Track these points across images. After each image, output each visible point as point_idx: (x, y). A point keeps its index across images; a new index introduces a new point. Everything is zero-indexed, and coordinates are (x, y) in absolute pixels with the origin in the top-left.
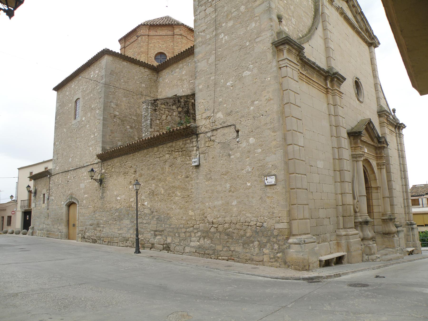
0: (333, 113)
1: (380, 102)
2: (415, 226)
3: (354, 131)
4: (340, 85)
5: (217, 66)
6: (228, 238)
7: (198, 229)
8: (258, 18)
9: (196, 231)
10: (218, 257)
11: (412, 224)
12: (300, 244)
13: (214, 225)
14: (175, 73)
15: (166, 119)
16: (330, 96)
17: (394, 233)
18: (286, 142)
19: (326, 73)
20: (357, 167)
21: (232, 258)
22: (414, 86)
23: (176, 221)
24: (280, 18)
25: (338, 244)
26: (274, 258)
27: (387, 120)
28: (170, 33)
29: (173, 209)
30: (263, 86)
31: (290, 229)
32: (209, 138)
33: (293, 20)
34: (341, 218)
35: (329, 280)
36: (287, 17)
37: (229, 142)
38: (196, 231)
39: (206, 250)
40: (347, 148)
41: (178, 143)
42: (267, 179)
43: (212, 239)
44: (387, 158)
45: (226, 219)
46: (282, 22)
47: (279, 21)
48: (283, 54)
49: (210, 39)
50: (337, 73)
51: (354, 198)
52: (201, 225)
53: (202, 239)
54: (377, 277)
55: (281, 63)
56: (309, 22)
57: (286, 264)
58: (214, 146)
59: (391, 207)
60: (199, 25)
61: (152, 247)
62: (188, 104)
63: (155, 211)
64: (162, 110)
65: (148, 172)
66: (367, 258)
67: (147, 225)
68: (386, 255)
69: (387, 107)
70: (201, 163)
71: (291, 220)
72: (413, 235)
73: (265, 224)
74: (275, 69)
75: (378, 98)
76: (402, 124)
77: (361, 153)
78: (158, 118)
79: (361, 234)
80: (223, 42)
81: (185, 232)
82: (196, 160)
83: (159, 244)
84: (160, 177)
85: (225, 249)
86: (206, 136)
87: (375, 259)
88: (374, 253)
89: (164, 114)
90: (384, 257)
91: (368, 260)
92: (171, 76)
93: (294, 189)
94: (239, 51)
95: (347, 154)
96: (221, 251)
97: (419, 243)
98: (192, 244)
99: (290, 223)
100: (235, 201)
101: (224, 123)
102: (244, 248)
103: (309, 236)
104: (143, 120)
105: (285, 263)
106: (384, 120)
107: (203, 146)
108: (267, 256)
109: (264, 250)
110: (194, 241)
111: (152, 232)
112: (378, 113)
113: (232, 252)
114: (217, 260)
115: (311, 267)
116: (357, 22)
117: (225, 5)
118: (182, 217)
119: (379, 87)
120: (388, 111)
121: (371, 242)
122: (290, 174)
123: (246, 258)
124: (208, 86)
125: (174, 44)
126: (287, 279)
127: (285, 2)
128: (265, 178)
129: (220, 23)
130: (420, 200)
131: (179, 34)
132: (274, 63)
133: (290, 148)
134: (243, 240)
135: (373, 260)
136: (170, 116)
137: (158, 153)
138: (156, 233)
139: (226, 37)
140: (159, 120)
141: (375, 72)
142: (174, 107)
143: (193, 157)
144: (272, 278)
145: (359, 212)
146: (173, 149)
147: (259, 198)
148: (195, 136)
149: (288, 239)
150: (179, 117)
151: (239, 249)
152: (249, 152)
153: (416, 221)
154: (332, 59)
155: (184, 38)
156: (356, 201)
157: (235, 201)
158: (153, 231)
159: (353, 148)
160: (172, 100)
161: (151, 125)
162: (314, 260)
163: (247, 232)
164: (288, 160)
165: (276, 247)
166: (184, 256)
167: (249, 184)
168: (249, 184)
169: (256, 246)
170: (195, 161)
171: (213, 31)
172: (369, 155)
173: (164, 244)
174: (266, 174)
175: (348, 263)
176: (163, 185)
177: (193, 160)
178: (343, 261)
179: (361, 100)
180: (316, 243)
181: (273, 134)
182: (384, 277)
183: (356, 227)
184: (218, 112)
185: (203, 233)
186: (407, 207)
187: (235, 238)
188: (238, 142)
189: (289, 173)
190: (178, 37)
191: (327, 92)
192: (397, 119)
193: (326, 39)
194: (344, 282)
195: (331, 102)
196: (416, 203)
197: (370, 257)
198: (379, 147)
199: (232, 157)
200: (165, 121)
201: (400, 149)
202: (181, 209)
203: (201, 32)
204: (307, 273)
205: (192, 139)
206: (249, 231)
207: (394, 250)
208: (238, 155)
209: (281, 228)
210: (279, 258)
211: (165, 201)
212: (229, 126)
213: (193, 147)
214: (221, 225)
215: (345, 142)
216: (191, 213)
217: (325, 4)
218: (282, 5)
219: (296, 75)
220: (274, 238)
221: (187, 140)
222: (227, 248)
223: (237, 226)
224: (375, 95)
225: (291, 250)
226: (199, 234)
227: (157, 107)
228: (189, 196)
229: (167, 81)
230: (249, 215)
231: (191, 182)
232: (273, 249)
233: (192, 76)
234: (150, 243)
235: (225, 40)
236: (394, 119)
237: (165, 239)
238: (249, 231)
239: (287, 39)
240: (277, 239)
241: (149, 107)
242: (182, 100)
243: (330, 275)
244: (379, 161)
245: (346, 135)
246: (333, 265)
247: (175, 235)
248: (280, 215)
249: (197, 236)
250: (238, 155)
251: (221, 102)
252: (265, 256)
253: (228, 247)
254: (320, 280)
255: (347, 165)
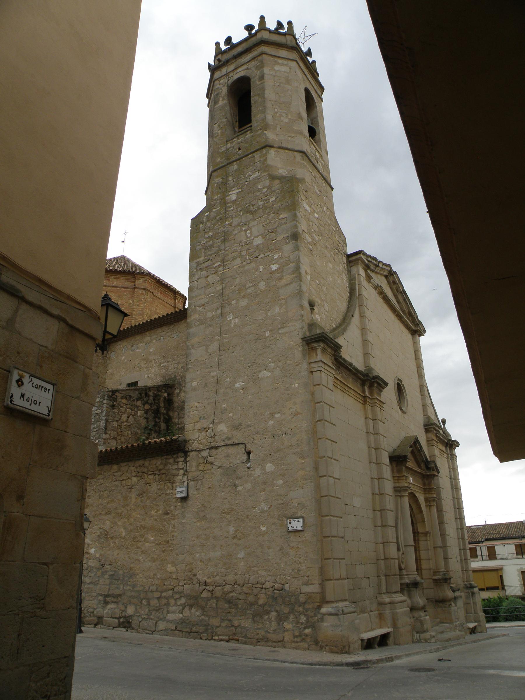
0: (372, 430)
1: (427, 411)
2: (476, 590)
3: (397, 454)
4: (381, 391)
5: (221, 357)
6: (230, 607)
7: (181, 593)
8: (283, 302)
9: (177, 596)
10: (212, 636)
11: (472, 587)
12: (337, 615)
13: (207, 588)
14: (138, 348)
15: (127, 421)
16: (369, 407)
17: (450, 600)
18: (318, 473)
19: (364, 376)
20: (401, 504)
21: (236, 637)
22: (495, 454)
23: (145, 580)
24: (312, 305)
25: (381, 616)
26: (300, 636)
27: (437, 436)
28: (130, 284)
29: (139, 560)
30: (288, 395)
31: (323, 593)
32: (204, 458)
33: (326, 306)
34: (383, 578)
35: (380, 665)
36: (319, 301)
37: (236, 468)
38: (177, 596)
39: (194, 625)
40: (389, 478)
41: (154, 461)
42: (290, 523)
43: (203, 608)
44: (438, 491)
45: (227, 578)
46: (314, 309)
47: (311, 309)
48: (317, 355)
49: (212, 318)
50: (377, 377)
51: (399, 549)
52: (187, 586)
53: (187, 608)
54: (440, 660)
55: (313, 365)
56: (343, 306)
57: (318, 644)
58: (212, 471)
59: (445, 562)
60: (196, 296)
61: (99, 621)
62: (159, 400)
63: (107, 563)
64: (122, 407)
65: (100, 501)
66: (418, 638)
67: (91, 586)
68: (442, 632)
69: (436, 418)
70: (190, 494)
71: (324, 579)
72: (475, 603)
73: (287, 587)
74: (306, 373)
75: (424, 406)
76: (455, 441)
77: (406, 485)
78: (116, 419)
79: (409, 601)
80: (232, 326)
81: (158, 598)
82: (183, 489)
83: (112, 617)
84: (119, 511)
85: (224, 624)
86: (200, 456)
87: (429, 639)
88: (427, 629)
89: (124, 413)
90: (440, 636)
91: (419, 641)
92: (131, 353)
93: (329, 537)
94: (254, 342)
95: (388, 487)
96: (217, 627)
97: (482, 615)
98: (170, 616)
99: (322, 585)
100: (243, 553)
101: (229, 439)
102: (254, 621)
103: (347, 603)
104: (93, 420)
105: (317, 643)
106: (432, 436)
107: (194, 469)
108: (289, 633)
109: (285, 624)
110: (173, 612)
111: (101, 598)
112: (425, 426)
113: (236, 629)
114: (212, 642)
115: (351, 649)
116: (398, 302)
117: (238, 276)
118: (155, 574)
119: (427, 394)
120: (438, 424)
121: (422, 614)
122: (322, 516)
123: (257, 637)
124: (206, 384)
125: (133, 301)
126: (326, 665)
127: (318, 282)
128: (288, 521)
129: (227, 300)
130: (478, 549)
131: (142, 287)
132: (305, 366)
133: (323, 480)
134: (253, 609)
135: (426, 641)
136: (133, 416)
137: (120, 473)
138: (108, 599)
139: (237, 320)
140: (117, 421)
141: (421, 370)
142: (139, 403)
143: (177, 484)
144: (303, 664)
145: (404, 569)
146: (145, 470)
147: (278, 548)
148: (183, 455)
149: (319, 607)
150: (145, 418)
151: (246, 623)
152: (265, 483)
153: (477, 581)
154: (371, 356)
155: (150, 294)
156: (401, 553)
157: (243, 553)
158: (102, 595)
159: (396, 478)
160: (137, 392)
161: (106, 429)
162: (354, 638)
163: (259, 598)
164: (321, 498)
165: (303, 619)
166: (157, 636)
167: (264, 529)
168: (264, 529)
169: (273, 619)
170: (180, 491)
171: (218, 309)
172: (415, 487)
173: (120, 618)
174: (290, 515)
175: (395, 644)
176: (125, 523)
177: (178, 489)
178: (388, 642)
179: (404, 409)
180: (356, 614)
181: (300, 461)
182: (450, 660)
183: (402, 591)
184: (220, 423)
185: (190, 599)
186: (464, 561)
187: (240, 606)
188: (248, 468)
189: (321, 515)
190: (140, 291)
191: (365, 402)
192: (449, 434)
193: (363, 330)
194: (402, 667)
195: (370, 416)
196: (474, 554)
197: (422, 636)
198: (428, 475)
199: (239, 488)
200: (125, 423)
201: (453, 477)
202: (154, 562)
203: (199, 307)
204: (350, 656)
205: (177, 457)
206: (262, 596)
207: (452, 626)
208: (249, 486)
209: (310, 591)
210: (307, 635)
211: (127, 548)
212: (236, 444)
213: (178, 469)
214: (220, 588)
215: (387, 471)
216: (170, 568)
217: (362, 283)
218: (314, 286)
219: (331, 382)
220: (300, 606)
221: (169, 459)
222: (227, 622)
223: (245, 589)
224: (420, 401)
225: (325, 624)
226: (183, 600)
227: (116, 401)
228: (168, 542)
229: (123, 359)
230: (264, 573)
231: (172, 522)
232: (298, 622)
233: (164, 357)
234: (94, 616)
235: (235, 323)
236: (444, 433)
237: (123, 608)
238: (262, 596)
239: (323, 336)
240: (304, 609)
241: (105, 401)
242: (151, 393)
243: (380, 658)
244: (427, 496)
245: (387, 461)
246: (376, 646)
247: (141, 602)
248: (309, 573)
249: (179, 603)
250: (249, 486)
251: (225, 409)
252: (286, 633)
253: (230, 620)
254: (369, 665)
255: (390, 503)
